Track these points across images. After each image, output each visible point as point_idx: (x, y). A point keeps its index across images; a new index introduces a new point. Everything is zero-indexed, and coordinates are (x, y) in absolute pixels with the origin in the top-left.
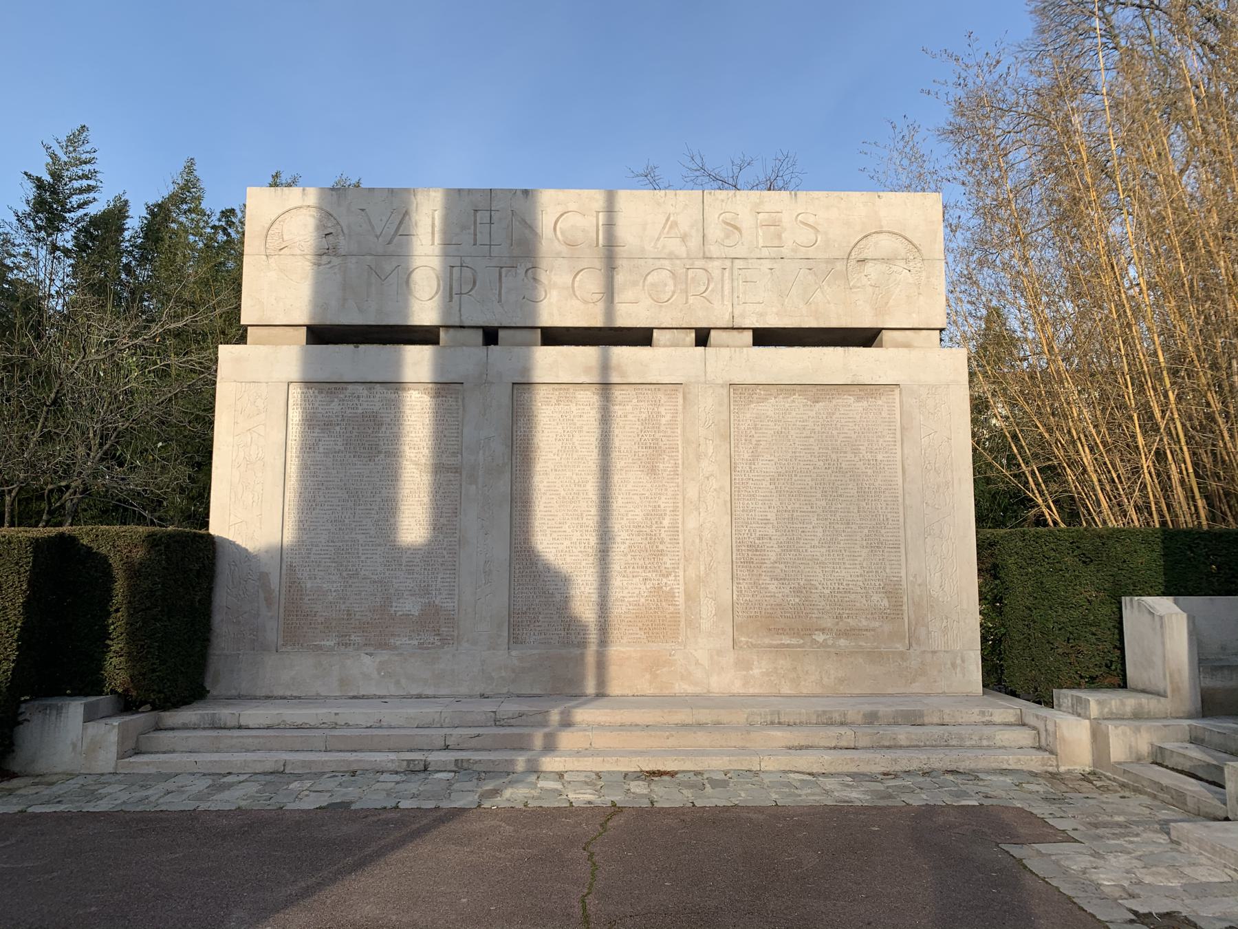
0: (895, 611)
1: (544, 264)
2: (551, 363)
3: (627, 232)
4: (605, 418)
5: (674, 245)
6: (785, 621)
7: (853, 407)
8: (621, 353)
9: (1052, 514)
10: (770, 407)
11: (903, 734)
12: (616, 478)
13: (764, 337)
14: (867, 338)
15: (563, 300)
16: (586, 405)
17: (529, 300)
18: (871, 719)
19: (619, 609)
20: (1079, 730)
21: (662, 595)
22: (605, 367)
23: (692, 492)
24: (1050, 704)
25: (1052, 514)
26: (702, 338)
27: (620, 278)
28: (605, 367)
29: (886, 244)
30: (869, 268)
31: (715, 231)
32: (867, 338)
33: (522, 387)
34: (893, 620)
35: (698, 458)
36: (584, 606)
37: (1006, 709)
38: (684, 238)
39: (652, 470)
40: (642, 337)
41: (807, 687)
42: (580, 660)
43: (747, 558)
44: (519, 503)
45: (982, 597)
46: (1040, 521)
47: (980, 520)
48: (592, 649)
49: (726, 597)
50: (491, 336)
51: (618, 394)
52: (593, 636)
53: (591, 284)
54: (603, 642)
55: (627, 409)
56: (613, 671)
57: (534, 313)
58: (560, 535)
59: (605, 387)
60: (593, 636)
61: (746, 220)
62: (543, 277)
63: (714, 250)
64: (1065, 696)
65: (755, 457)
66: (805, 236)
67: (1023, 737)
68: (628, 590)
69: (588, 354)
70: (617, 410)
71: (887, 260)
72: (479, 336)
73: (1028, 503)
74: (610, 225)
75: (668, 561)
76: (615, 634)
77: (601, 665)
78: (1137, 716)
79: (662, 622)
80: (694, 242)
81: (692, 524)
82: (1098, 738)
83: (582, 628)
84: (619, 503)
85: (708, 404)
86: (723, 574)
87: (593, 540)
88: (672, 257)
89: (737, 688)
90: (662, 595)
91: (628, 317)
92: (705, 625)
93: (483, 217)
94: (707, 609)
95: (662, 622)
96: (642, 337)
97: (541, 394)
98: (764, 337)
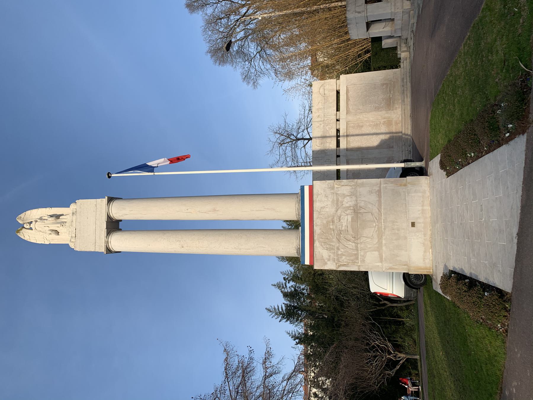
0: (387, 84)
1: (325, 148)
2: (343, 145)
3: (319, 135)
4: (353, 135)
5: (322, 126)
6: (389, 104)
7: (350, 93)
8: (341, 133)
9: (368, 55)
10: (350, 107)
11: (405, 81)
12: (363, 133)
13: (338, 109)
14: (338, 93)
15: (332, 145)
16: (351, 139)
17: (332, 150)
18: (403, 86)
19: (387, 131)
20: (403, 54)
21: (384, 123)
22: (344, 136)
23: (366, 119)
24: (400, 58)
25: (368, 55)
26: (337, 120)
27: (328, 135)
28: (344, 136)
29: (322, 90)
30: (326, 93)
31: (319, 119)
32: (338, 93)
33: (347, 150)
34: (388, 85)
35: (359, 118)
36: (387, 137)
37: (402, 64)
38: (320, 124)
39: (362, 126)
40: (338, 131)
41: (400, 98)
42: (396, 136)
43: (377, 109)
44: (368, 149)
45: (384, 70)
46: (369, 57)
47: (371, 71)
48: (394, 135)
49: (384, 112)
50: (338, 156)
51: (348, 134)
52: (392, 135)
53: (328, 140)
54: (393, 133)
55: (352, 131)
56: (398, 131)
57: (334, 150)
58: (375, 141)
59: (347, 136)
60: (392, 135)
61: (317, 114)
62: (327, 148)
63: (323, 119)
64: (399, 56)
65: (359, 109)
66: (320, 104)
67: (405, 62)
68: (383, 129)
69: (341, 139)
70: (351, 133)
71: (324, 90)
72: (338, 158)
73: (366, 61)
74: (318, 137)
75: (378, 123)
76: (391, 131)
77: (396, 133)
78: (400, 46)
79: (389, 123)
80: (321, 123)
81: (372, 119)
82: (403, 52)
83: (391, 137)
84: (368, 132)
85: (350, 118)
86: (380, 113)
87: (374, 136)
88: (324, 126)
89: (400, 109)
90: (384, 123)
91: (334, 133)
92: (389, 115)
93: (317, 159)
94: (387, 115)
95: (389, 123)
96: (338, 131)
97: (349, 147)
98: (338, 109)
